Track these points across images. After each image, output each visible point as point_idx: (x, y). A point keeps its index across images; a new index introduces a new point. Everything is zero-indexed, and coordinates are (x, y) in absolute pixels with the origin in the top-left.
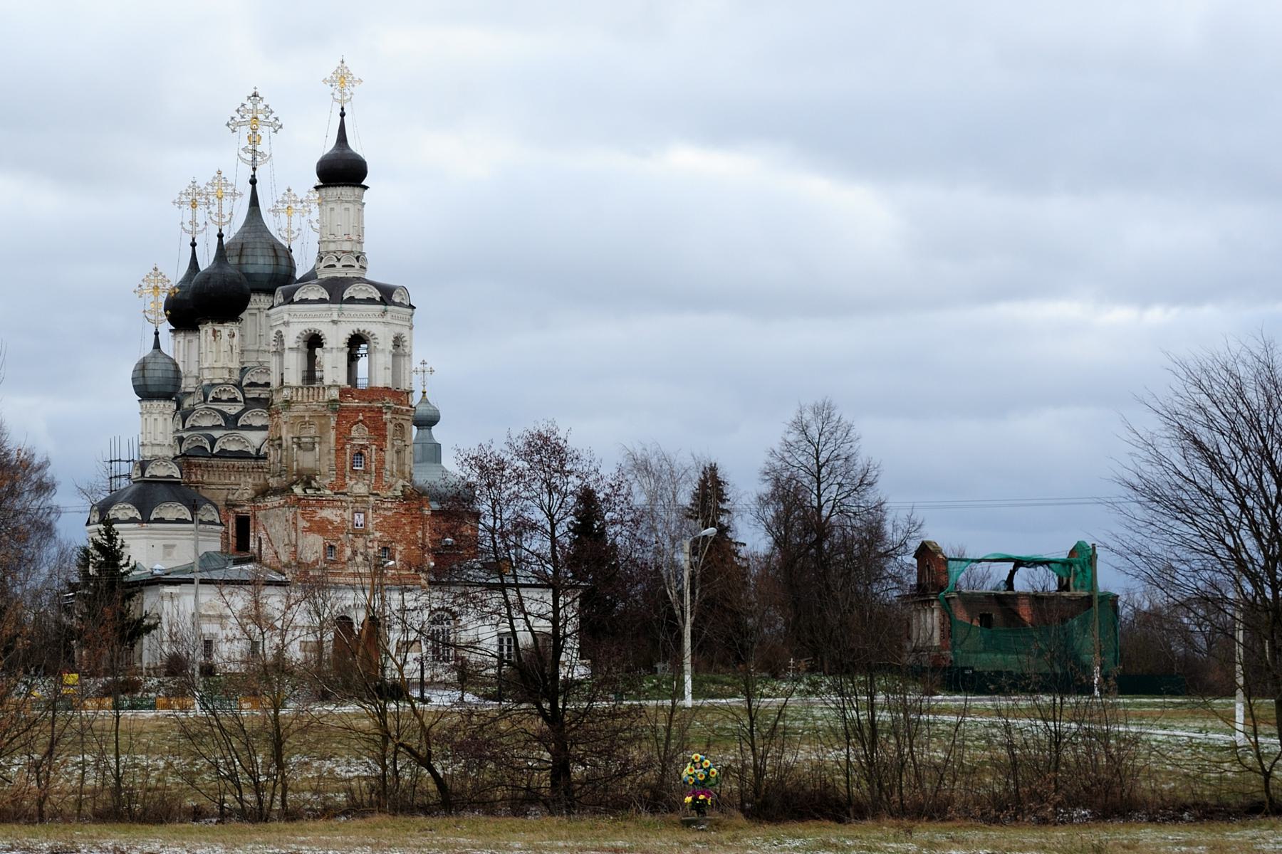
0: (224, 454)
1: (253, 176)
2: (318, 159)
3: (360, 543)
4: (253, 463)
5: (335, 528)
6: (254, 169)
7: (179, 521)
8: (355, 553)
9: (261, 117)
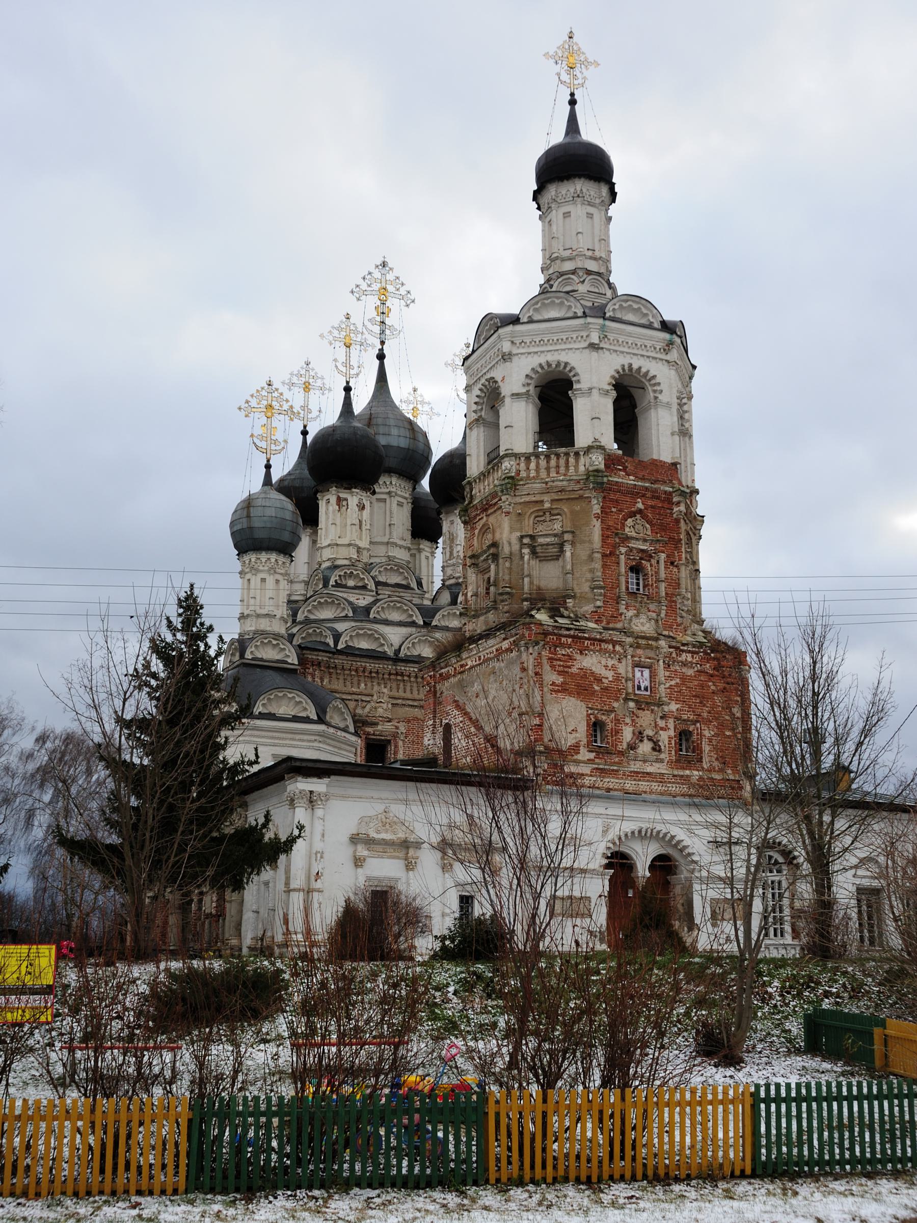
0: (350, 652)
1: (381, 350)
2: (541, 152)
3: (646, 718)
4: (390, 667)
5: (606, 689)
6: (383, 343)
7: (295, 719)
8: (639, 735)
9: (390, 288)
